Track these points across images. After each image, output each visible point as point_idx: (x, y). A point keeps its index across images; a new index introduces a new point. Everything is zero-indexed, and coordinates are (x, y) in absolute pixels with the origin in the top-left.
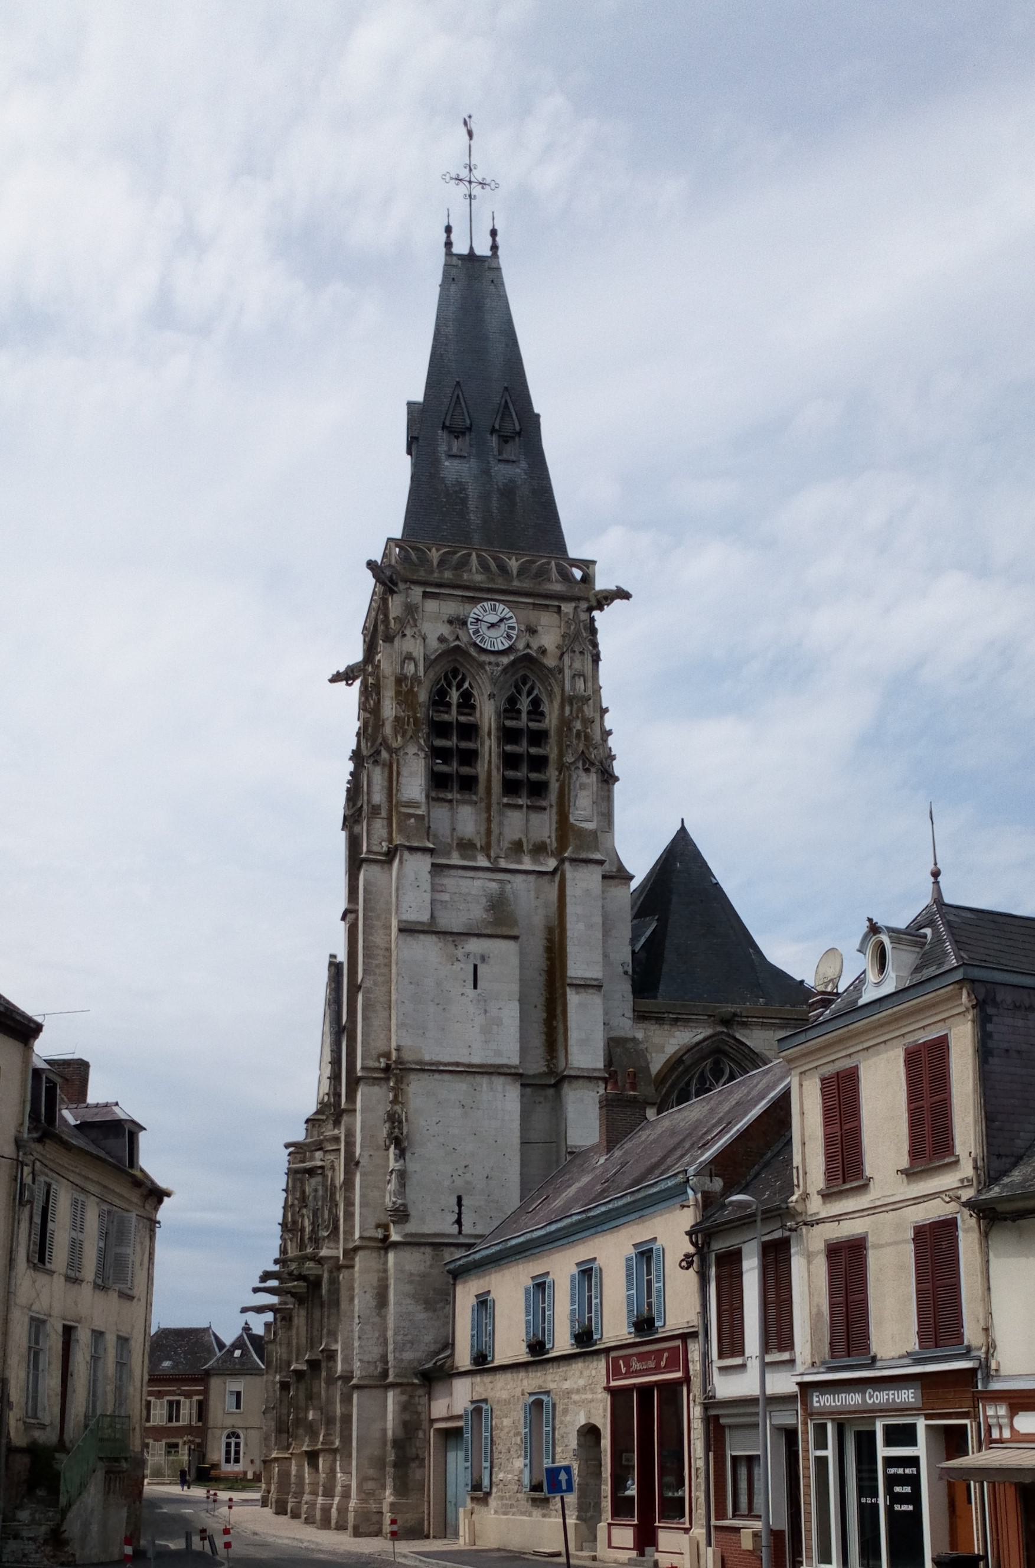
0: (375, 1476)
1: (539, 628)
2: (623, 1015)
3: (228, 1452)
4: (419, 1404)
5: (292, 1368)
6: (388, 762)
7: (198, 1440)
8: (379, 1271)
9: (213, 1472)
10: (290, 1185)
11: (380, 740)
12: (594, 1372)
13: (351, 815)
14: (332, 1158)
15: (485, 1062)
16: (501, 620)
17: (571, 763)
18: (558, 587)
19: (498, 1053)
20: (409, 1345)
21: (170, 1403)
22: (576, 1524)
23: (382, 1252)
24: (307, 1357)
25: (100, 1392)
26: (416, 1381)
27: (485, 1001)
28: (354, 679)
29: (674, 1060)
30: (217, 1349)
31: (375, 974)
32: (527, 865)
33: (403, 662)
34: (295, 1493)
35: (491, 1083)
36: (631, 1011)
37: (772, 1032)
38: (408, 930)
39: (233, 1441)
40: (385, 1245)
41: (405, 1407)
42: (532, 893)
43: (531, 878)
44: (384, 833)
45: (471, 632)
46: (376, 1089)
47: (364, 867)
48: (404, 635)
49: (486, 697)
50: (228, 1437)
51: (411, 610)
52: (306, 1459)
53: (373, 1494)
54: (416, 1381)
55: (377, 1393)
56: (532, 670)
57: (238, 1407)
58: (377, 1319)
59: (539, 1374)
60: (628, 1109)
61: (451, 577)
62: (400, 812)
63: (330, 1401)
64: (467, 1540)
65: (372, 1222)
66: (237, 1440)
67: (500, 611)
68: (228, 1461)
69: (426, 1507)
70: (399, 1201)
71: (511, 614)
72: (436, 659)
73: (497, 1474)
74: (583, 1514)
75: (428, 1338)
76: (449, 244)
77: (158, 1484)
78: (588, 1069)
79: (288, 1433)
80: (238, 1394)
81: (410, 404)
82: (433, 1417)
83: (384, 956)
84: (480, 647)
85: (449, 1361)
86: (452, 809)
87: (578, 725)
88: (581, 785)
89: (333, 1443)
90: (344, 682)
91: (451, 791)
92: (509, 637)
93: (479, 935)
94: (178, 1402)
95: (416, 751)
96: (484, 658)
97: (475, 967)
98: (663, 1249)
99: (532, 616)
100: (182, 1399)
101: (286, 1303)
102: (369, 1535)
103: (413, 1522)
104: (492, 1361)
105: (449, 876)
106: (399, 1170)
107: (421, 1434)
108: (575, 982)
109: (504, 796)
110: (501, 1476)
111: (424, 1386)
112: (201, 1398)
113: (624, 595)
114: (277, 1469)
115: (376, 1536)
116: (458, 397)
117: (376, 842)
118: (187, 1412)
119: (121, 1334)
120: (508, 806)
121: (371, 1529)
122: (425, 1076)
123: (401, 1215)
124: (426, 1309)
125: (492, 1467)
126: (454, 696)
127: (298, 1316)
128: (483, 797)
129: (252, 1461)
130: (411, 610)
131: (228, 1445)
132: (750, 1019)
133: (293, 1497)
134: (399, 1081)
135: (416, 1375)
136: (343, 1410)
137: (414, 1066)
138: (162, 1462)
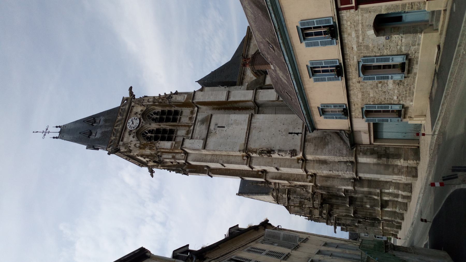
1: (136, 111)
2: (240, 88)
4: (364, 149)
5: (353, 215)
6: (161, 153)
8: (314, 163)
10: (299, 214)
11: (155, 155)
12: (349, 23)
13: (183, 171)
14: (281, 186)
15: (247, 125)
16: (132, 121)
17: (169, 101)
18: (127, 106)
19: (245, 121)
20: (340, 151)
22: (424, 33)
23: (307, 162)
24: (348, 206)
25: (349, 256)
26: (355, 149)
27: (229, 124)
28: (153, 170)
29: (255, 74)
31: (219, 160)
32: (195, 115)
33: (136, 147)
34: (395, 218)
35: (254, 123)
36: (239, 86)
37: (250, 49)
38: (204, 147)
40: (304, 160)
41: (365, 154)
42: (203, 114)
43: (199, 114)
44: (179, 155)
45: (133, 129)
46: (253, 161)
47: (188, 161)
48: (130, 147)
49: (150, 126)
51: (124, 144)
52: (383, 209)
54: (355, 149)
55: (359, 166)
56: (147, 114)
58: (331, 165)
59: (350, 70)
60: (256, 59)
61: (119, 134)
62: (173, 149)
63: (363, 193)
64: (423, 119)
65: (297, 165)
67: (130, 122)
69: (406, 147)
70: (289, 152)
71: (131, 119)
72: (138, 139)
73: (394, 101)
74: (418, 31)
75: (339, 145)
76: (57, 138)
78: (253, 95)
79: (374, 223)
81: (87, 149)
82: (369, 143)
83: (214, 156)
84: (138, 126)
85: (346, 132)
86: (177, 136)
87: (160, 100)
88: (175, 99)
89: (378, 193)
90: (153, 173)
91: (173, 136)
92: (137, 119)
93: (209, 126)
95: (158, 143)
96: (140, 126)
97: (218, 127)
98: (310, 61)
99: (133, 113)
101: (334, 219)
103: (412, 152)
104: (346, 105)
105: (194, 137)
106: (278, 151)
107: (376, 149)
108: (227, 99)
109: (177, 122)
110: (395, 98)
111: (356, 146)
113: (131, 88)
114: (386, 228)
115: (417, 169)
116: (83, 133)
117: (182, 158)
119: (323, 245)
120: (179, 121)
121: (414, 171)
122: (249, 143)
123: (293, 152)
124: (328, 145)
125: (391, 104)
126: (149, 135)
128: (176, 128)
130: (124, 144)
132: (246, 54)
133: (396, 219)
134: (250, 151)
135: (352, 149)
136: (366, 187)
137: (245, 146)
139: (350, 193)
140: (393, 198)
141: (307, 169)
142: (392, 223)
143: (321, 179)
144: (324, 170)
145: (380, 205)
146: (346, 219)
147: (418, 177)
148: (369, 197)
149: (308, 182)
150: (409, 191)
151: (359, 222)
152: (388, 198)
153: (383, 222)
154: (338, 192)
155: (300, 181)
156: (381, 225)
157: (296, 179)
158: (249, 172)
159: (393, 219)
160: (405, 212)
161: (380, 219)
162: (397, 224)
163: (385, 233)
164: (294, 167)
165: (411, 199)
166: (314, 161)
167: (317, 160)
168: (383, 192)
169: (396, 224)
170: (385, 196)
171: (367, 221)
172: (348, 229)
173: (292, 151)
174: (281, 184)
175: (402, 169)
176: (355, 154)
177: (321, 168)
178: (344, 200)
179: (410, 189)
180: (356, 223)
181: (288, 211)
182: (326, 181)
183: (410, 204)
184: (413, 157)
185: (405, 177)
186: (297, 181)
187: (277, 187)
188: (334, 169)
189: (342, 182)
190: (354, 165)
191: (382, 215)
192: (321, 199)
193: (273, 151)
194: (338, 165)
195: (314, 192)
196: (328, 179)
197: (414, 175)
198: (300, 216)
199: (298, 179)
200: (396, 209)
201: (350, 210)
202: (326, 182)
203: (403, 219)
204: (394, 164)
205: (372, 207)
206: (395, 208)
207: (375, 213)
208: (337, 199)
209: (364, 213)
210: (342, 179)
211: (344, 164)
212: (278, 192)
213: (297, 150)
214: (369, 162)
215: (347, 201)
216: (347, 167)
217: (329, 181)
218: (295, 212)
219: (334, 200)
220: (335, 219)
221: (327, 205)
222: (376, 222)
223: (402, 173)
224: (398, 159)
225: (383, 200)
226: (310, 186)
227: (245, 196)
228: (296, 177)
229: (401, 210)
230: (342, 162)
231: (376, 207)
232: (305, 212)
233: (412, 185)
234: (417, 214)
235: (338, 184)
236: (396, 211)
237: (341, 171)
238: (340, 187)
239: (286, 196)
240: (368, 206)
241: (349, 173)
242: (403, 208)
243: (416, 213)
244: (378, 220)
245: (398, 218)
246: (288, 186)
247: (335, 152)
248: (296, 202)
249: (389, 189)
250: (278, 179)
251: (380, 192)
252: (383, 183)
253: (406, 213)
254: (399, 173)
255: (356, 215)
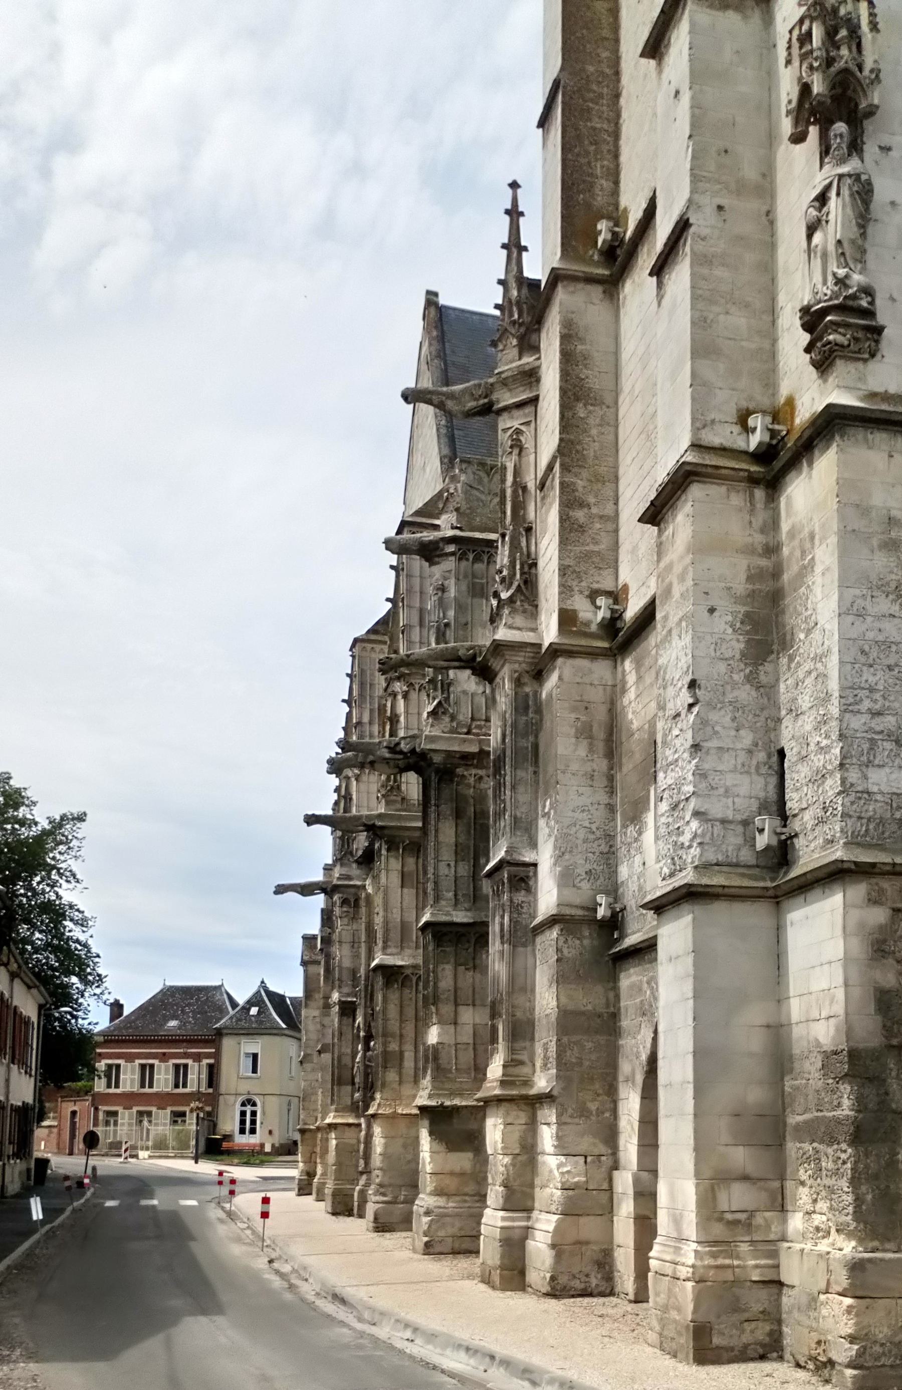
0: (751, 1170)
3: (243, 1122)
7: (208, 1109)
9: (225, 1145)
10: (355, 693)
14: (516, 424)
21: (177, 1067)
23: (759, 494)
30: (230, 1009)
34: (381, 1185)
39: (248, 1109)
50: (243, 1104)
52: (426, 1123)
53: (748, 1226)
57: (254, 1070)
58: (745, 694)
66: (254, 1108)
68: (242, 1131)
77: (160, 1157)
79: (353, 1084)
80: (255, 1056)
89: (527, 1083)
94: (186, 1066)
100: (190, 1062)
101: (349, 878)
102: (742, 1356)
112: (212, 1061)
114: (334, 1142)
115: (762, 1358)
118: (195, 1077)
121: (746, 1338)
127: (387, 871)
129: (270, 1132)
131: (243, 1114)
136: (563, 1000)
138: (167, 1132)
139: (511, 901)
140: (500, 1179)
141: (696, 491)
142: (362, 1173)
143: (597, 696)
144: (697, 638)
145: (448, 1103)
146: (354, 943)
147: (695, 1368)
148: (494, 1030)
149: (561, 600)
150: (563, 1280)
151: (348, 1009)
152: (500, 1146)
153: (363, 1126)
154: (506, 821)
155: (564, 542)
156: (342, 1116)
157: (579, 515)
158: (605, 148)
159: (377, 1176)
160: (422, 1245)
161: (371, 1111)
162: (356, 1194)
163: (315, 1138)
164: (704, 384)
165: (504, 1289)
166: (772, 550)
167: (776, 573)
168: (539, 1113)
169: (358, 1188)
170: (507, 1124)
171: (360, 1047)
172: (312, 969)
173: (869, 313)
174: (527, 423)
175: (752, 1242)
176: (873, 865)
177: (712, 611)
178: (456, 895)
179: (577, 1285)
180: (340, 993)
181: (369, 632)
182: (584, 732)
183: (470, 1277)
184: (882, 1333)
185: (693, 1266)
186: (564, 519)
187: (508, 394)
188: (714, 716)
189: (585, 841)
190: (757, 871)
191: (394, 1116)
192: (449, 754)
193: (855, 147)
194: (750, 752)
195: (495, 664)
196: (600, 746)
197: (717, 1340)
198: (344, 701)
199: (581, 529)
200: (431, 1194)
201: (402, 948)
202: (573, 731)
203: (382, 1226)
204: (789, 1184)
205: (434, 1054)
206: (436, 1189)
207: (401, 1082)
208: (459, 851)
209: (394, 1026)
210: (610, 838)
211: (762, 795)
212: (471, 404)
213: (873, 365)
214: (795, 982)
215: (454, 913)
216: (739, 817)
217: (582, 752)
218: (362, 672)
219: (452, 832)
220: (352, 883)
221: (414, 818)
222: (357, 1095)
223: (716, 1243)
224: (858, 1215)
225: (484, 1119)
226: (534, 630)
227: (425, 348)
228: (594, 510)
229: (426, 1220)
230: (773, 781)
231: (434, 1079)
232: (371, 723)
233: (602, 1295)
234: (399, 1339)
235: (570, 814)
236: (421, 1196)
237: (700, 774)
238: (543, 828)
239: (450, 533)
240: (433, 1036)
241: (685, 839)
242: (442, 1233)
243: (408, 1334)
244: (367, 1100)
245: (383, 1202)
246: (517, 473)
247: (877, 696)
248: (417, 640)
249: (563, 1149)
250: (565, 375)
251: (533, 1091)
252: (600, 1112)
253: (414, 1251)
254: (720, 1219)
255: (380, 981)
